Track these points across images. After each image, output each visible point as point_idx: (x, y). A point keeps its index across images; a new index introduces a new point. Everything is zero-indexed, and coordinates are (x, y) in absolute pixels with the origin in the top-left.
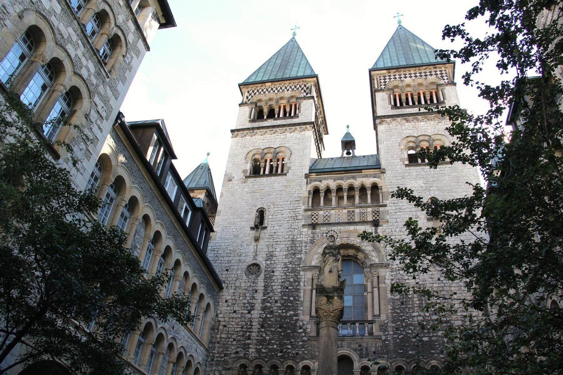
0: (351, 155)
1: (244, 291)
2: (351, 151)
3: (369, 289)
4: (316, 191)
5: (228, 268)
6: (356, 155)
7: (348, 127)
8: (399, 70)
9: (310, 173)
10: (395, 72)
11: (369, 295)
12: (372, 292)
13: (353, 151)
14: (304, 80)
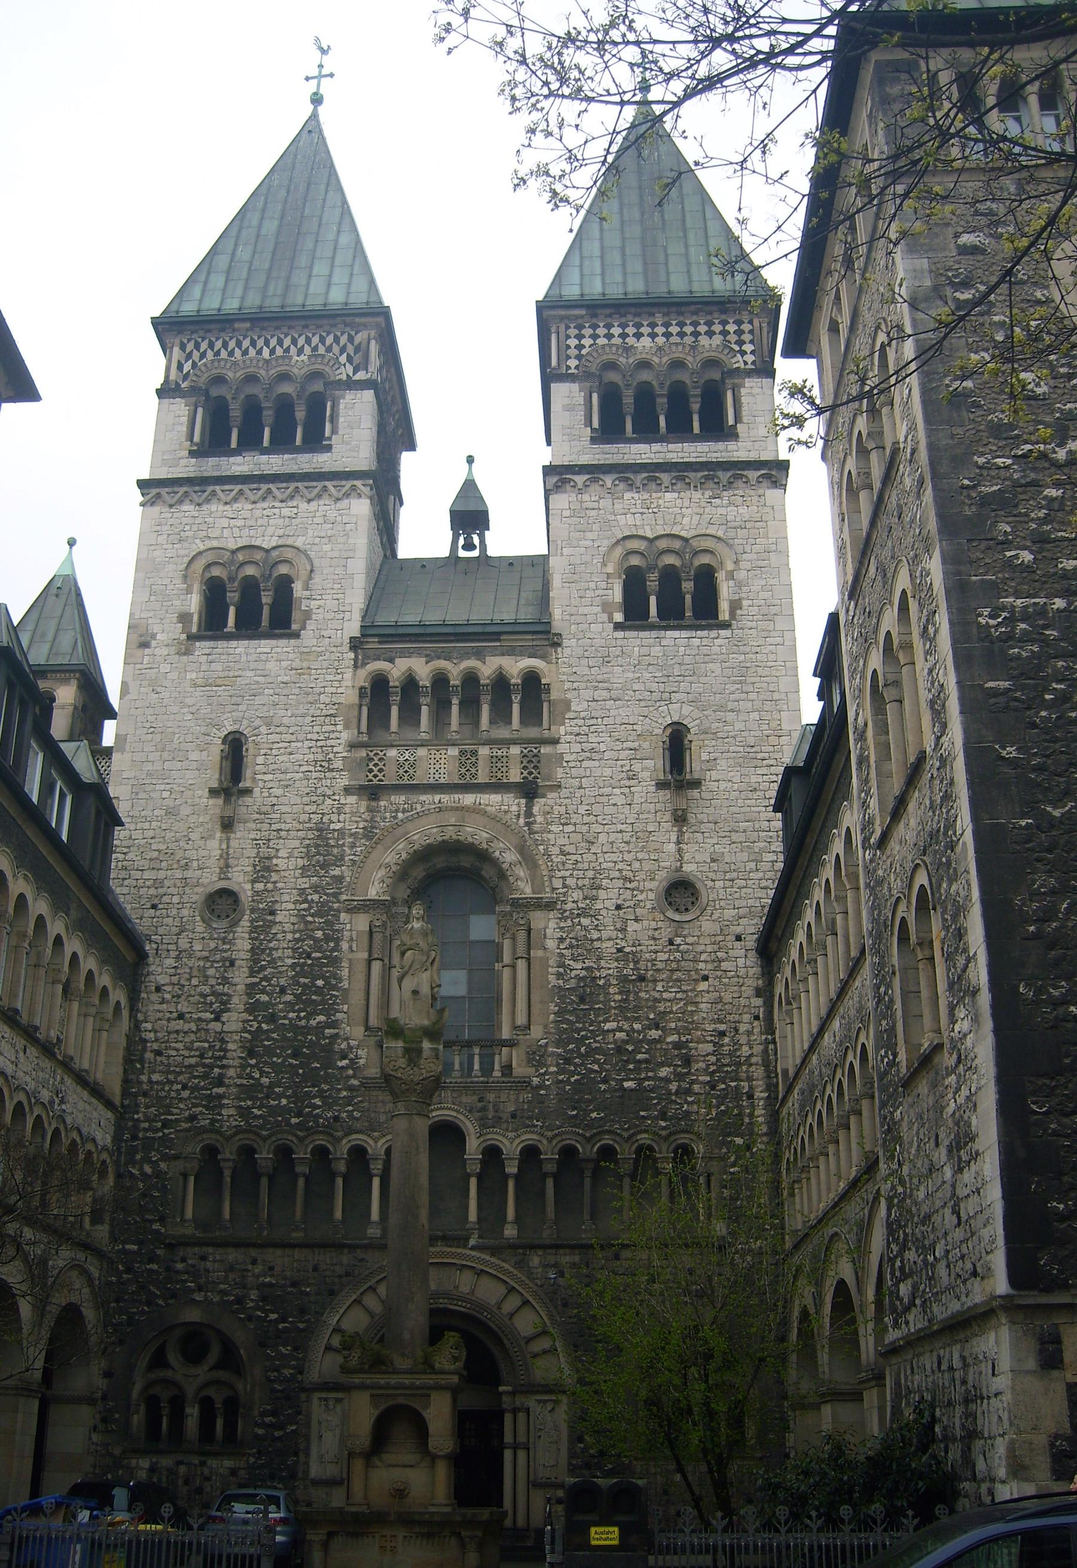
0: (475, 553)
1: (201, 963)
2: (476, 540)
5: (156, 901)
6: (490, 553)
7: (470, 460)
8: (622, 310)
10: (610, 316)
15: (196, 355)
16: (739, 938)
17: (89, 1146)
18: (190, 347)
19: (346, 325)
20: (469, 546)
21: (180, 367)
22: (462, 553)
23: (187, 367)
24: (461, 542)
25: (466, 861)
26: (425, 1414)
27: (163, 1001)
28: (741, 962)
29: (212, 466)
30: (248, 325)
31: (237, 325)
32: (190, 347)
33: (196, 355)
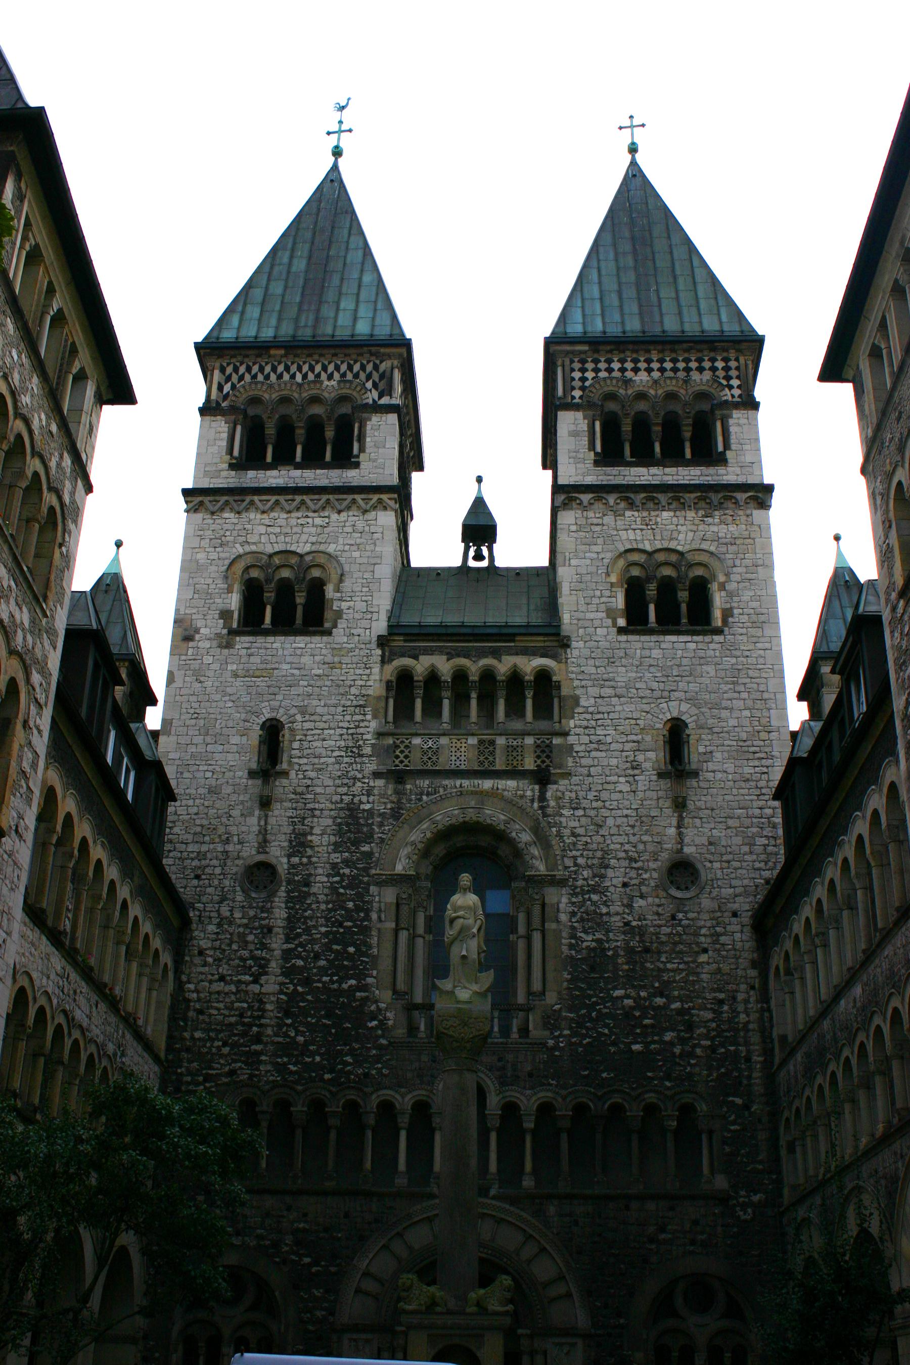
0: (484, 564)
2: (485, 551)
3: (522, 930)
4: (404, 679)
7: (479, 480)
10: (611, 351)
11: (521, 945)
12: (529, 938)
14: (373, 349)
15: (235, 378)
19: (371, 354)
20: (479, 557)
22: (472, 563)
23: (227, 388)
24: (472, 553)
25: (484, 841)
26: (478, 1355)
27: (205, 964)
28: (738, 936)
29: (253, 477)
30: (282, 352)
31: (273, 352)
32: (229, 370)
33: (235, 378)
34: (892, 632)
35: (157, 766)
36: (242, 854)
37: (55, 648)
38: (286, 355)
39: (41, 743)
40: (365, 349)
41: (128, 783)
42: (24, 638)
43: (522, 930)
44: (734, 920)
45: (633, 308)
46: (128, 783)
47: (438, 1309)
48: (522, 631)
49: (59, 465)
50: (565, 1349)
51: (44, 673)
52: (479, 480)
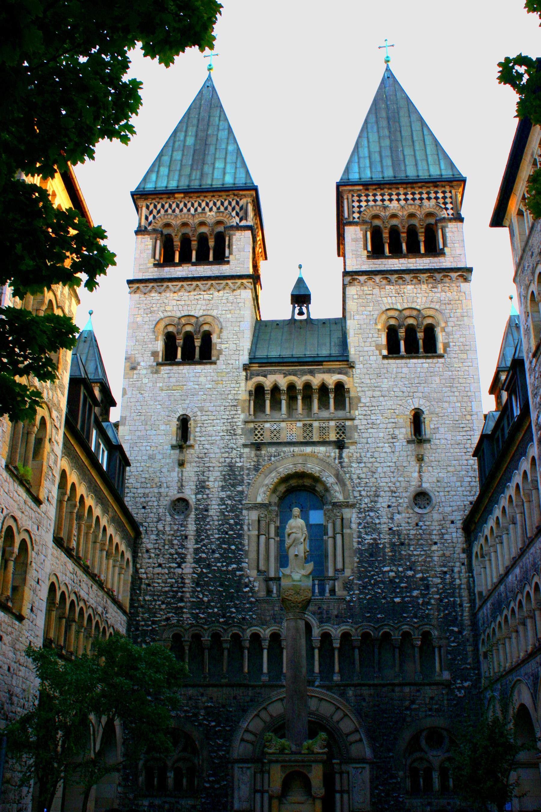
0: (304, 317)
2: (304, 309)
3: (330, 533)
5: (145, 505)
7: (300, 267)
9: (250, 363)
10: (375, 189)
11: (330, 542)
12: (334, 538)
13: (307, 308)
14: (236, 192)
15: (155, 212)
16: (452, 522)
17: (63, 588)
18: (151, 207)
20: (301, 313)
21: (147, 218)
22: (297, 317)
23: (151, 218)
24: (297, 311)
25: (308, 482)
28: (454, 535)
30: (182, 195)
31: (176, 195)
32: (151, 207)
33: (155, 212)
34: (530, 375)
35: (119, 448)
36: (170, 494)
37: (63, 395)
38: (184, 198)
39: (59, 449)
40: (231, 193)
41: (103, 459)
42: (48, 394)
43: (330, 533)
44: (452, 525)
45: (388, 162)
46: (103, 459)
47: (286, 751)
48: (327, 359)
49: (62, 292)
50: (360, 771)
51: (59, 410)
52: (300, 267)
